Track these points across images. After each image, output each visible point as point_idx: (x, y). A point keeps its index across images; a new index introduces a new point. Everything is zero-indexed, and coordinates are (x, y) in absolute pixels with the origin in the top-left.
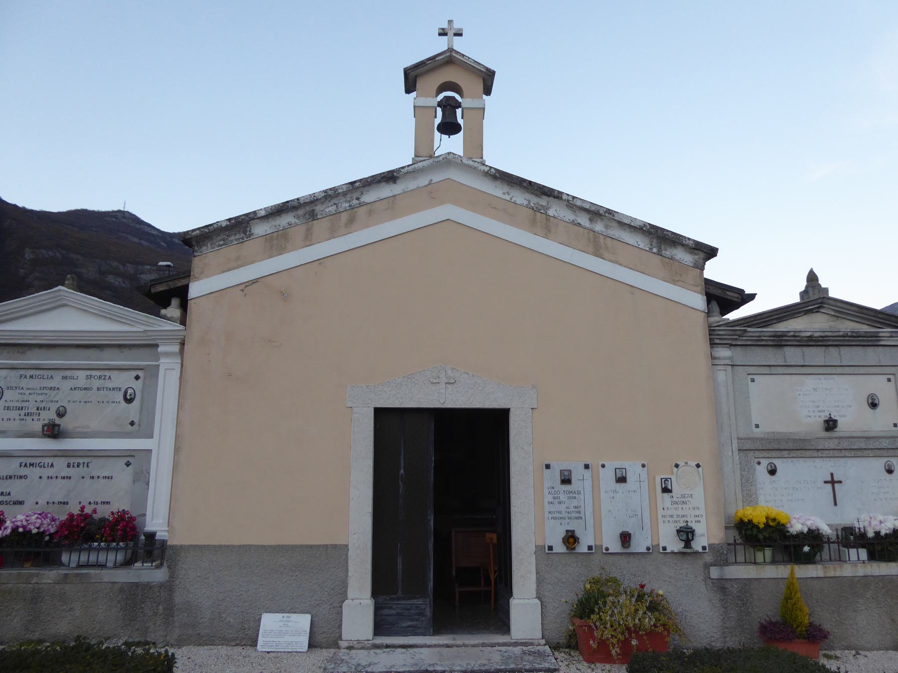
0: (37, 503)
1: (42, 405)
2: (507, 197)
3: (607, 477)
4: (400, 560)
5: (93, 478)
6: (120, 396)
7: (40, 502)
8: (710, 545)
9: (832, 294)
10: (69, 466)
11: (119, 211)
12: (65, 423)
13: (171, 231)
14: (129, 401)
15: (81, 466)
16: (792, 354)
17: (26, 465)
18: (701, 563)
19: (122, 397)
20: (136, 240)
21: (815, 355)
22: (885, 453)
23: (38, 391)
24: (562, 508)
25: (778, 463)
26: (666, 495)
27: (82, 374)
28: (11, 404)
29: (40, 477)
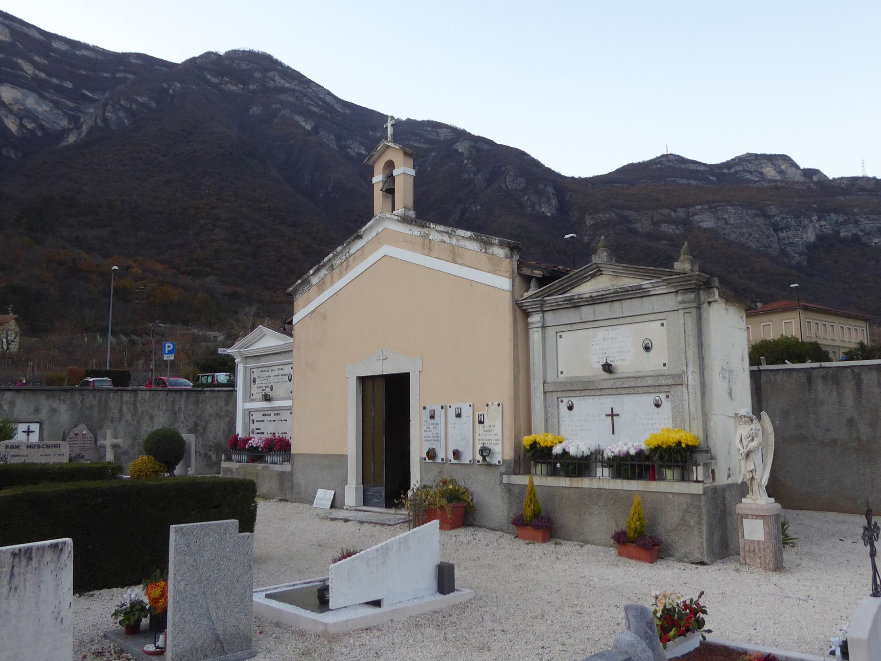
2: (410, 233)
3: (452, 413)
6: (287, 378)
11: (663, 156)
12: (271, 394)
13: (719, 162)
16: (587, 313)
18: (499, 472)
20: (684, 181)
21: (603, 311)
22: (651, 389)
24: (430, 434)
25: (575, 401)
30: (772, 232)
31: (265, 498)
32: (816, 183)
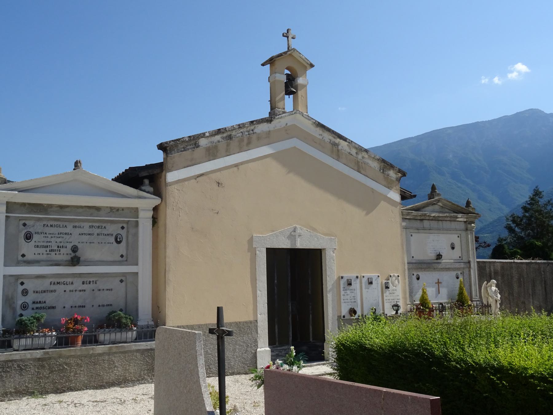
0: (64, 307)
1: (61, 245)
4: (276, 327)
5: (100, 290)
6: (112, 239)
7: (66, 306)
10: (83, 283)
14: (119, 242)
15: (92, 283)
17: (54, 283)
19: (114, 240)
21: (434, 224)
23: (57, 235)
24: (348, 297)
25: (421, 274)
27: (87, 225)
28: (40, 244)
29: (65, 291)
31: (227, 375)
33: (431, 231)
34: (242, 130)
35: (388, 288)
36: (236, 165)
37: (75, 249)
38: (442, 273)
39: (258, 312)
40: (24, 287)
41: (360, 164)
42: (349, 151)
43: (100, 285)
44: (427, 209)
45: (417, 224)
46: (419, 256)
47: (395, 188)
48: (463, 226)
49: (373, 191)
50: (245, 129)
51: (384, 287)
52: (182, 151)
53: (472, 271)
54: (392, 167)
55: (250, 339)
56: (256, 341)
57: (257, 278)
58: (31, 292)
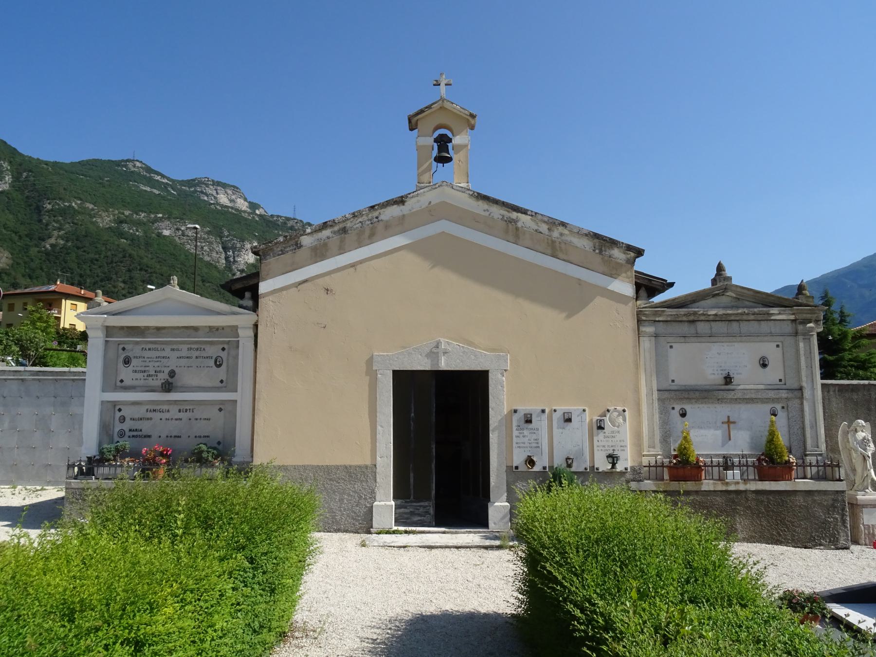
1: (158, 369)
4: (412, 475)
6: (211, 363)
8: (631, 467)
9: (734, 282)
10: (180, 411)
21: (718, 327)
25: (688, 408)
26: (600, 431)
28: (138, 369)
30: (221, 250)
32: (260, 216)
33: (712, 339)
34: (360, 220)
35: (603, 428)
36: (353, 266)
37: (172, 374)
38: (737, 406)
39: (378, 453)
40: (121, 413)
41: (557, 244)
42: (536, 228)
43: (198, 414)
44: (702, 303)
45: (685, 328)
46: (683, 377)
47: (624, 275)
48: (788, 328)
49: (579, 281)
50: (365, 218)
51: (595, 427)
52: (279, 255)
53: (806, 404)
54: (613, 243)
55: (365, 489)
56: (373, 492)
57: (378, 410)
58: (127, 419)
